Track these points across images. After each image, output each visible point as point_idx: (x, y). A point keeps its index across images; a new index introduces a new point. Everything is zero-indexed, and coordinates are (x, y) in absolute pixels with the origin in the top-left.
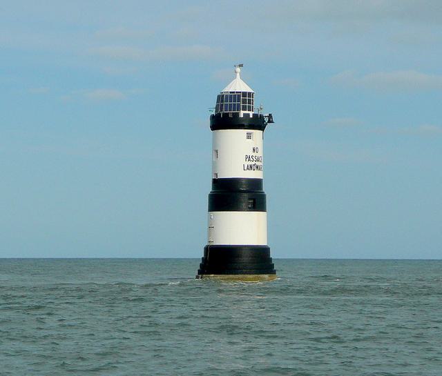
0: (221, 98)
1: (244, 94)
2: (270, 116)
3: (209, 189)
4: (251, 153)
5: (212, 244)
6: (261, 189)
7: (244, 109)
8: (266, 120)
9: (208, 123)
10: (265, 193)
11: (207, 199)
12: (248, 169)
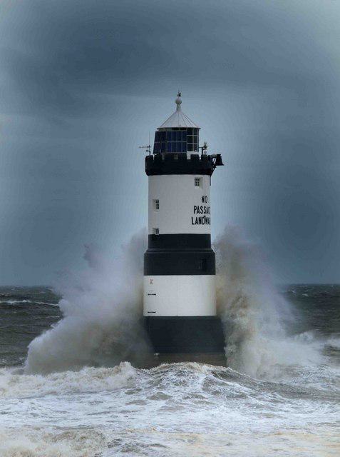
2: (219, 157)
4: (200, 204)
6: (210, 247)
7: (190, 149)
8: (214, 160)
12: (196, 223)
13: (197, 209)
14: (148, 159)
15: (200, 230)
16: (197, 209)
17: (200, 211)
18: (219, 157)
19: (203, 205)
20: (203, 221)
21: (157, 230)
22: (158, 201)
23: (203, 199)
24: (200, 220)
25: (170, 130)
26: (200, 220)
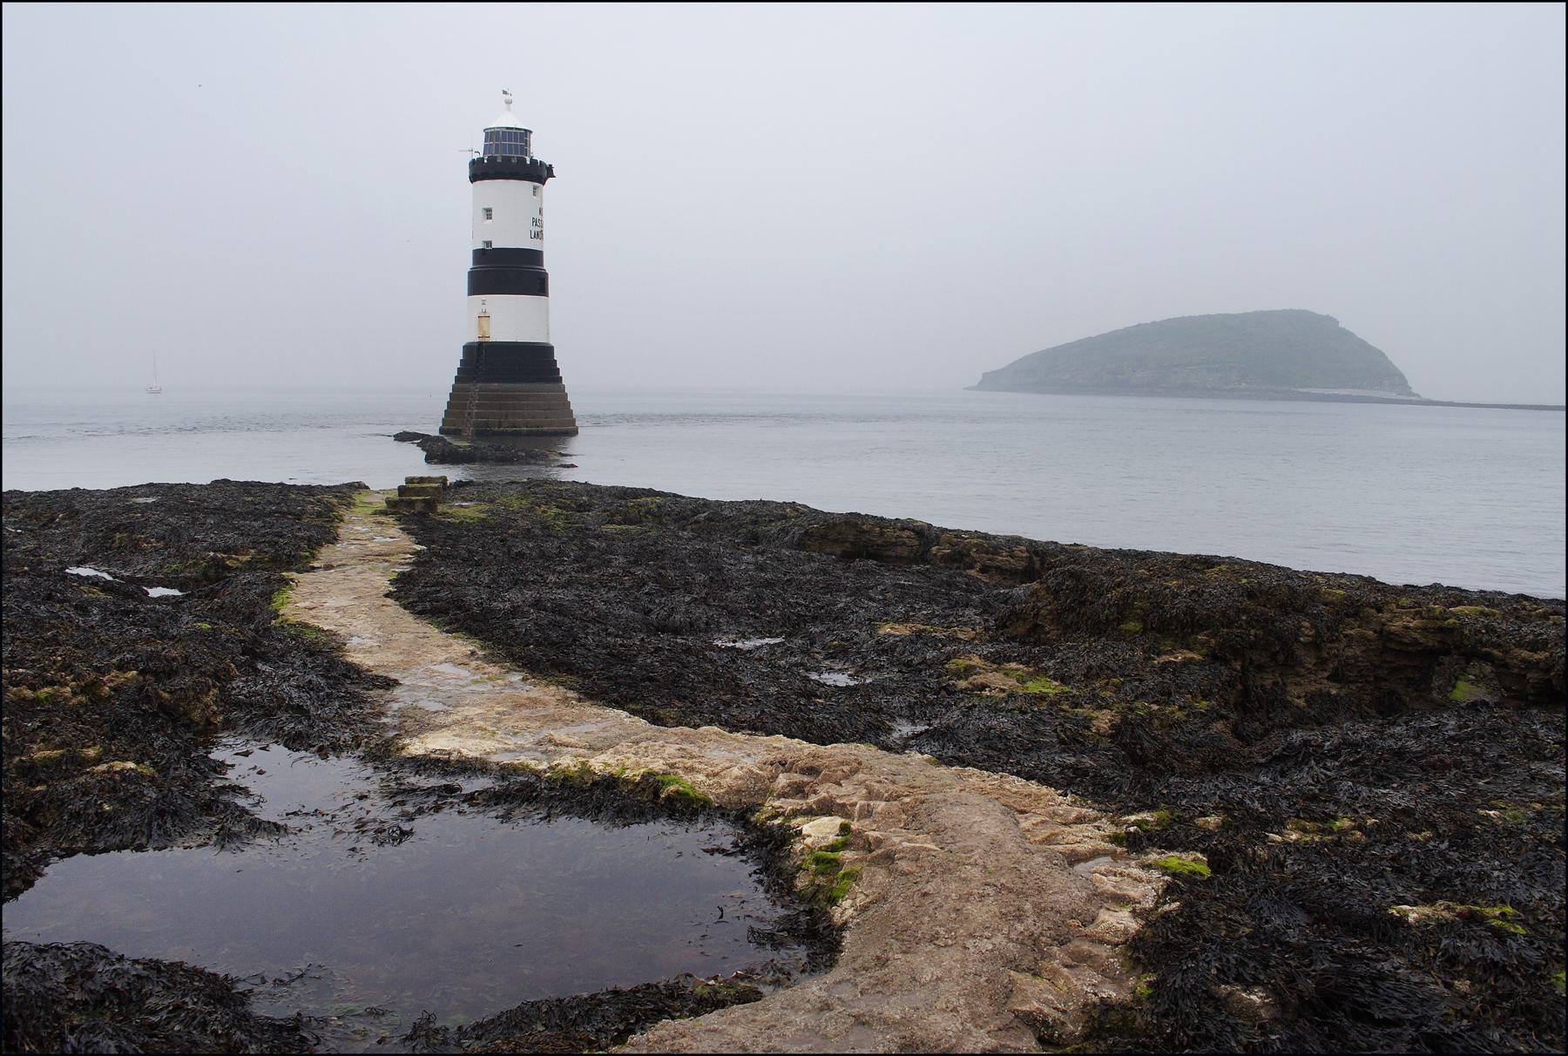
0: (492, 135)
2: (550, 168)
3: (469, 264)
4: (537, 216)
5: (487, 340)
6: (542, 265)
9: (466, 172)
11: (467, 274)
14: (475, 164)
16: (535, 222)
25: (504, 130)
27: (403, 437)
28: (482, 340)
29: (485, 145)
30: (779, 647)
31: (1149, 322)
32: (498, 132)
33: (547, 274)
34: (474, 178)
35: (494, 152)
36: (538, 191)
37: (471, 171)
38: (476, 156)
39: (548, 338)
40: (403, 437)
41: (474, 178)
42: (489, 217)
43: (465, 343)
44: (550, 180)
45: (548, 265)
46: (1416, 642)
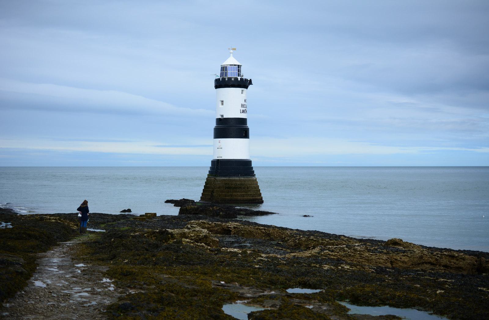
1: (238, 66)
2: (251, 81)
3: (214, 125)
4: (244, 103)
6: (246, 125)
9: (213, 84)
10: (249, 127)
13: (243, 106)
14: (217, 81)
15: (243, 116)
16: (243, 106)
17: (244, 106)
18: (251, 81)
19: (245, 103)
20: (245, 111)
21: (222, 116)
22: (223, 101)
23: (245, 101)
24: (244, 111)
26: (244, 111)
27: (168, 202)
28: (218, 158)
29: (221, 73)
30: (174, 219)
31: (179, 200)
32: (226, 67)
33: (249, 128)
34: (217, 87)
35: (224, 76)
36: (244, 92)
37: (215, 84)
38: (217, 78)
39: (201, 179)
40: (168, 202)
41: (217, 87)
42: (222, 104)
43: (212, 159)
44: (250, 86)
45: (249, 125)
46: (226, 229)
